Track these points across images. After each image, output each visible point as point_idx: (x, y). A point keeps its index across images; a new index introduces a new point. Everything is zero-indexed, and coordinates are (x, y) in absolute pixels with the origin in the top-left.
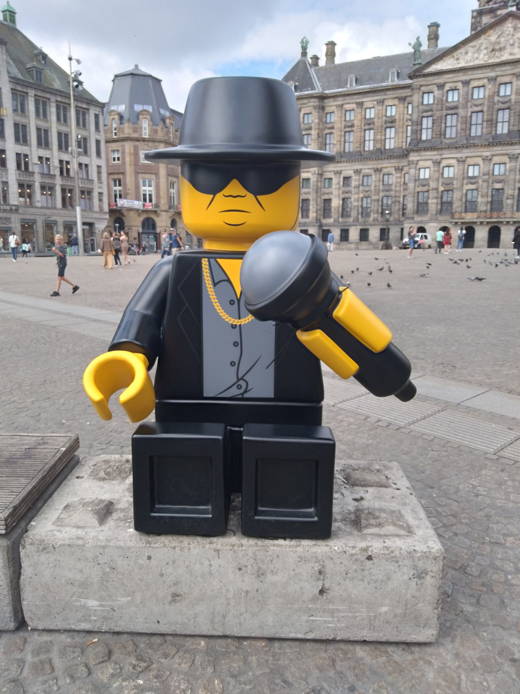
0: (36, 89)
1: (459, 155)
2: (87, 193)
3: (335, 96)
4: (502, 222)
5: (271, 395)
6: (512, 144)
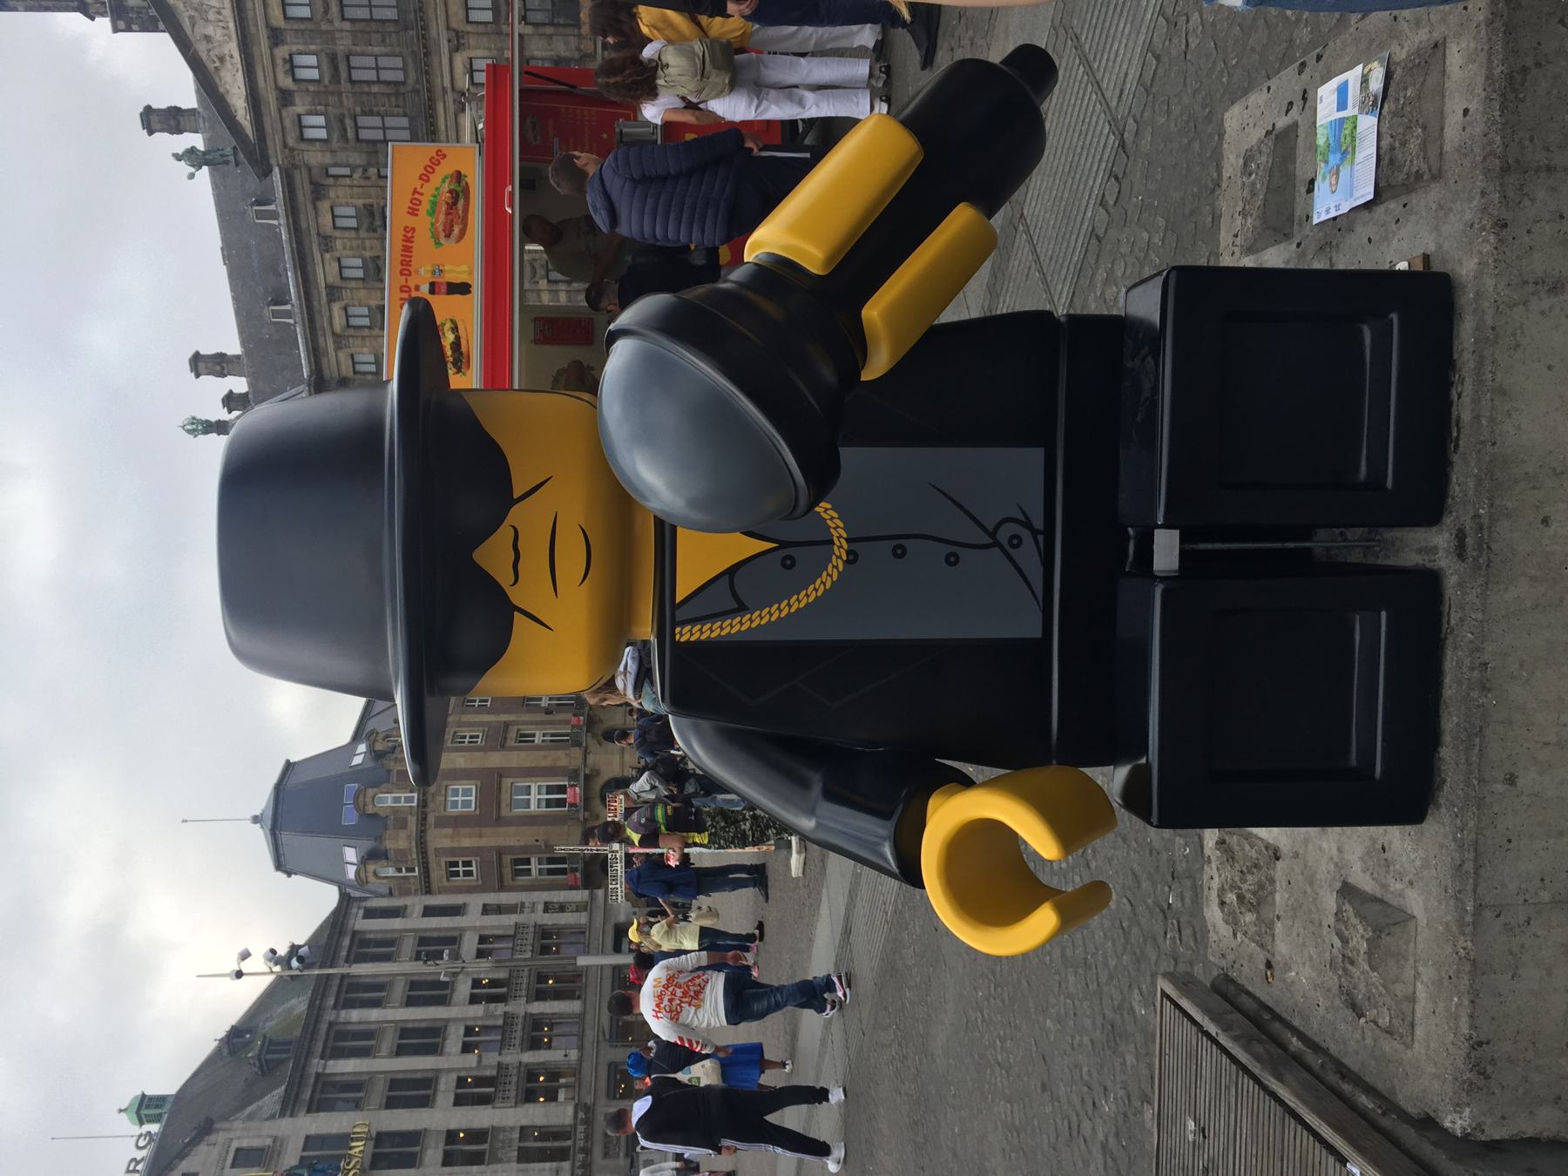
0: (309, 1054)
1: (445, 47)
2: (546, 939)
3: (316, 353)
5: (1037, 455)
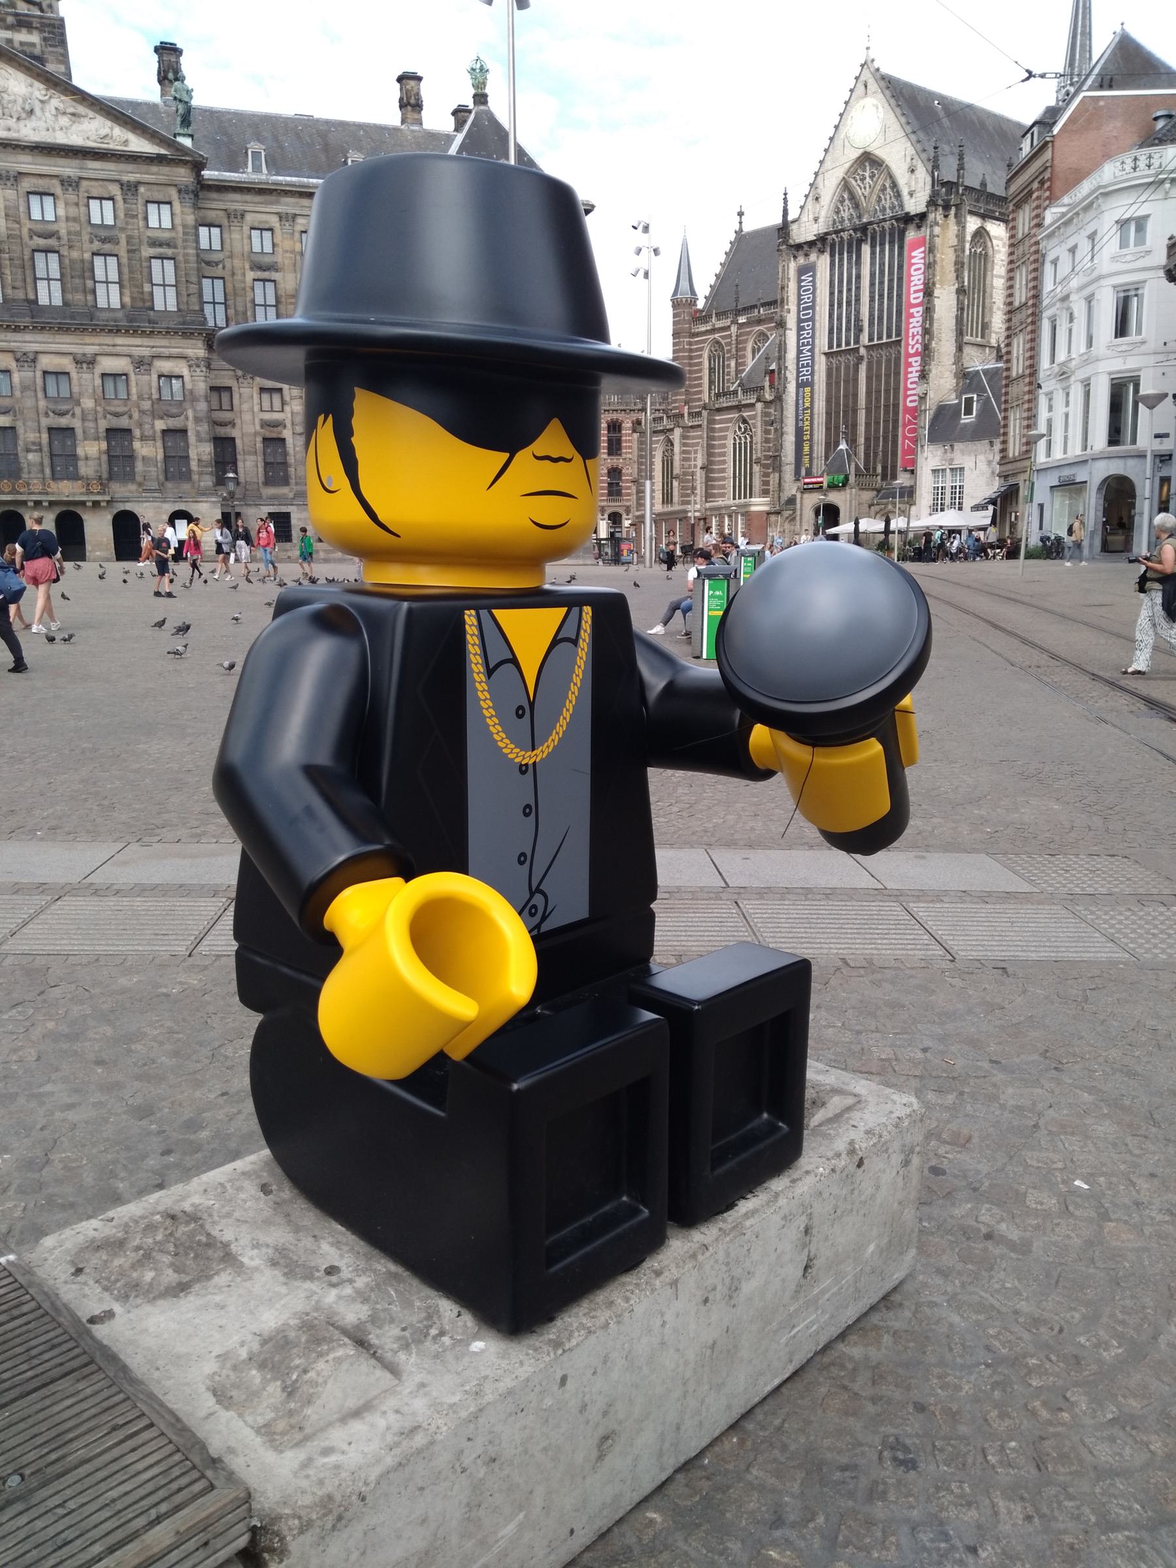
4: (24, 503)
6: (17, 329)
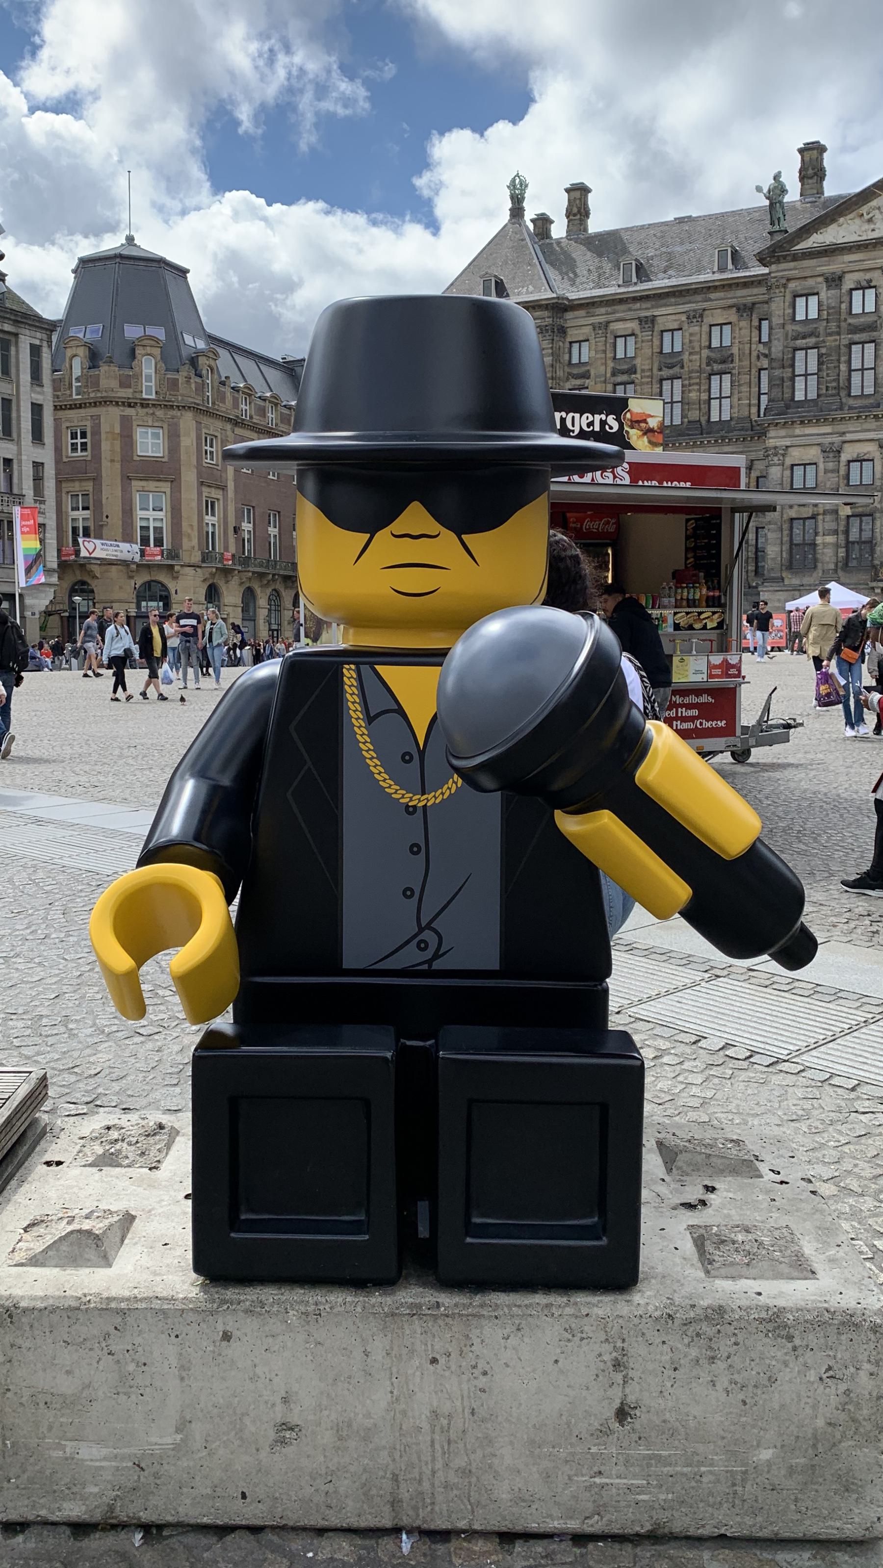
5: (495, 965)
